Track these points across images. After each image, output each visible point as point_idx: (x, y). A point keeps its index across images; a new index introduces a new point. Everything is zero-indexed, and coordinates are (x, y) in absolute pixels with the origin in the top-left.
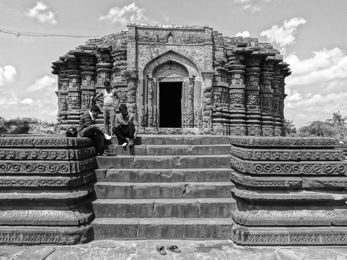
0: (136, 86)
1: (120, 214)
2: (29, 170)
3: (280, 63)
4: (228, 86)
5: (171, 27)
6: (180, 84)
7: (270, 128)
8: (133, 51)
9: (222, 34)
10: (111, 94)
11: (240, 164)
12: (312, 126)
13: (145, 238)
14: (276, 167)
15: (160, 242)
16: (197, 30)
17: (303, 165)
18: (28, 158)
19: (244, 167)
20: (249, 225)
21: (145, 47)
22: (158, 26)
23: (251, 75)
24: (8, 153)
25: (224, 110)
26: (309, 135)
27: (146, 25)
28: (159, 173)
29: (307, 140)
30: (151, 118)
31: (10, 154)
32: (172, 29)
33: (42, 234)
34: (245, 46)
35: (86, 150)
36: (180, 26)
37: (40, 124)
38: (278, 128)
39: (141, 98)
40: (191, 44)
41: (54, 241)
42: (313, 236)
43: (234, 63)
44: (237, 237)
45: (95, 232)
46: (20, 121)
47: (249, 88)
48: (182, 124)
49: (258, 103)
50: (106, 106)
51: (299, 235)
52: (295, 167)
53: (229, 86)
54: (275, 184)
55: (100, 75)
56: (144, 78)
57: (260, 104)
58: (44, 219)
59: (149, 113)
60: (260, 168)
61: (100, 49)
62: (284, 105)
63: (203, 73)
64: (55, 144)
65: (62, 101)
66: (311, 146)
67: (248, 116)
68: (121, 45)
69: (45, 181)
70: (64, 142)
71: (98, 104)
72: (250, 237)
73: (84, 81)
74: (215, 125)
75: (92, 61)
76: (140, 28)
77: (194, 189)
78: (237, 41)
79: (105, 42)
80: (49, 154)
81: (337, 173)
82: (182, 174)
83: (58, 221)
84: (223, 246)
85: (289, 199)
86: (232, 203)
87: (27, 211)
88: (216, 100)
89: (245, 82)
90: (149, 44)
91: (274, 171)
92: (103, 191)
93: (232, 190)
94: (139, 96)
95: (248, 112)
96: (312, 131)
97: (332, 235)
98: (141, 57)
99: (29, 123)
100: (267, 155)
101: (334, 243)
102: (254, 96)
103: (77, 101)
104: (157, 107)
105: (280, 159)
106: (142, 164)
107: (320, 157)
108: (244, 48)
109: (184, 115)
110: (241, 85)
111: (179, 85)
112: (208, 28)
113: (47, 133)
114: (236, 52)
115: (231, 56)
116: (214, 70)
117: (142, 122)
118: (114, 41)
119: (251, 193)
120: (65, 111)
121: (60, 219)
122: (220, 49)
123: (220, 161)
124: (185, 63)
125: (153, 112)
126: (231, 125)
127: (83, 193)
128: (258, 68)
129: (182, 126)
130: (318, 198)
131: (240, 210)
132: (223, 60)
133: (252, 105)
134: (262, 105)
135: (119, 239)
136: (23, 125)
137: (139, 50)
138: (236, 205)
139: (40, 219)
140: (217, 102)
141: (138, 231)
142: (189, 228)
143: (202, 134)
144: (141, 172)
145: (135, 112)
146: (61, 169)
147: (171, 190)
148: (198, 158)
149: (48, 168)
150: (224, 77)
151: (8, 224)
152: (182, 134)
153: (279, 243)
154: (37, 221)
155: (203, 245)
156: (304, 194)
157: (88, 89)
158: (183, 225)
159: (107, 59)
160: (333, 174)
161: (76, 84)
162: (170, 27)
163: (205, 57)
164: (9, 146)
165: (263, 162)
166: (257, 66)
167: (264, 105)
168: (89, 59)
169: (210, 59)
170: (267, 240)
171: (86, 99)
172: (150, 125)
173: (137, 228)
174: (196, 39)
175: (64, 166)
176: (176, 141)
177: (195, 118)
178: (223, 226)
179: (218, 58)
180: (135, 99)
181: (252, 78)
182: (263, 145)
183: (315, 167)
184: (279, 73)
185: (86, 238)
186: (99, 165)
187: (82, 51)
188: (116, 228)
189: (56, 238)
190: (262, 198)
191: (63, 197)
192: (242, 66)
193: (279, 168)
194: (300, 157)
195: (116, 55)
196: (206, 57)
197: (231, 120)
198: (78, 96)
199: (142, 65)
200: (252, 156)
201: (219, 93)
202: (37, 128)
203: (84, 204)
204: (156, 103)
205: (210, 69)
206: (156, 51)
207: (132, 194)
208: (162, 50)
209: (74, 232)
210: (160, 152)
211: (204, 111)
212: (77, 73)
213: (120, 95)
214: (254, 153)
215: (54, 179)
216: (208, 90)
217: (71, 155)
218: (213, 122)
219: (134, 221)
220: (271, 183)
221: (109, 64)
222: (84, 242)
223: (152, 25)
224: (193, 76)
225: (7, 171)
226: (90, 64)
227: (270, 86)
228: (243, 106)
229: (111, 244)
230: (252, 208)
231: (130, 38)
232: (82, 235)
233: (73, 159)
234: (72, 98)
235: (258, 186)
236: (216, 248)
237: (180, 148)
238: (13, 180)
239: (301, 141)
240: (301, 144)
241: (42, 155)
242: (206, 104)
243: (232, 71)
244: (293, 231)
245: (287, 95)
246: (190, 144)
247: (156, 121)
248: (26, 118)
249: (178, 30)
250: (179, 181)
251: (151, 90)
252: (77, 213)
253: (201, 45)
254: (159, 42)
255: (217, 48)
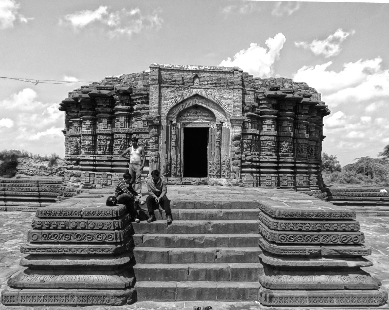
0: (159, 132)
1: (159, 277)
2: (78, 239)
3: (318, 105)
4: (259, 133)
5: (198, 69)
6: (207, 129)
7: (305, 178)
8: (155, 95)
9: (252, 76)
10: (138, 151)
11: (267, 232)
12: (359, 164)
13: (182, 300)
14: (299, 237)
15: (195, 303)
16: (225, 72)
17: (323, 235)
18: (77, 228)
19: (270, 236)
20: (274, 288)
21: (168, 90)
22: (183, 67)
23: (284, 120)
24: (59, 224)
25: (254, 159)
26: (356, 175)
27: (170, 66)
28: (192, 239)
29: (327, 213)
30: (175, 167)
31: (62, 225)
32: (199, 71)
33: (94, 296)
34: (277, 89)
35: (125, 218)
36: (207, 67)
37: (31, 158)
38: (314, 176)
39: (165, 145)
40: (219, 88)
41: (104, 302)
42: (329, 298)
43: (265, 107)
44: (263, 299)
45: (138, 294)
46: (7, 155)
47: (282, 134)
48: (209, 173)
49: (291, 150)
50: (132, 165)
51: (316, 298)
52: (316, 237)
53: (260, 132)
54: (297, 253)
55: (119, 119)
56: (167, 124)
57: (293, 151)
58: (94, 283)
59: (173, 162)
60: (285, 238)
61: (119, 91)
62: (322, 148)
63: (231, 120)
64: (101, 215)
65: (73, 144)
66: (330, 218)
67: (280, 165)
68: (142, 87)
69: (94, 249)
70: (109, 213)
71: (116, 151)
72: (275, 299)
73: (101, 124)
74: (244, 176)
75: (109, 103)
76: (163, 69)
77: (225, 255)
78: (269, 83)
79: (124, 82)
80: (96, 225)
81: (352, 243)
82: (214, 240)
83: (107, 285)
84: (251, 307)
85: (309, 265)
86: (260, 268)
87: (78, 276)
88: (245, 148)
89: (277, 129)
90: (173, 87)
91: (297, 240)
92: (142, 256)
93: (260, 256)
94: (161, 143)
95: (281, 160)
96: (359, 169)
97: (345, 297)
98: (164, 100)
99: (18, 157)
100: (291, 226)
101: (346, 304)
102: (287, 143)
103: (91, 145)
104: (181, 155)
105: (303, 230)
106: (176, 230)
107: (338, 228)
108: (276, 92)
109: (210, 164)
110: (273, 132)
111: (205, 131)
112: (237, 70)
113: (40, 169)
114: (268, 96)
115: (263, 99)
116: (243, 115)
117: (165, 172)
118: (135, 82)
119: (276, 260)
120: (76, 155)
121: (109, 283)
122: (250, 92)
123: (249, 226)
124: (213, 108)
125: (177, 161)
126: (262, 175)
127: (125, 260)
128: (292, 113)
129: (208, 176)
130: (334, 265)
131: (267, 275)
132: (253, 105)
133: (285, 153)
134: (296, 151)
135: (159, 300)
136: (10, 160)
137: (162, 93)
138: (263, 270)
139: (91, 283)
140: (246, 151)
141: (176, 294)
142: (221, 291)
143: (230, 185)
144: (176, 238)
145: (157, 162)
146: (107, 238)
147: (204, 255)
148: (228, 224)
149: (96, 237)
150: (254, 123)
151: (63, 287)
152: (208, 185)
153: (299, 304)
154: (88, 285)
155: (234, 305)
156: (323, 261)
157: (105, 133)
158: (216, 288)
159: (126, 102)
160: (349, 243)
161: (90, 126)
162: (196, 69)
163: (234, 102)
164: (59, 216)
165: (287, 233)
166: (291, 110)
167: (298, 151)
168: (106, 100)
169: (240, 104)
170: (289, 301)
171: (102, 145)
172: (173, 175)
173: (175, 291)
174: (224, 82)
175: (110, 235)
176: (206, 205)
177: (222, 168)
178: (251, 289)
179: (248, 103)
180: (158, 147)
181: (285, 124)
182: (288, 217)
183: (333, 238)
184: (315, 115)
185: (131, 300)
186: (135, 231)
187: (99, 92)
188: (157, 290)
189: (105, 300)
190: (285, 265)
191: (111, 263)
192: (275, 111)
193: (301, 238)
194: (320, 228)
195: (137, 98)
196: (235, 103)
197: (262, 170)
198: (92, 140)
199: (166, 109)
200: (277, 227)
201: (249, 141)
202: (27, 163)
203: (126, 270)
204: (180, 150)
205: (239, 115)
206: (181, 95)
207: (168, 259)
208: (187, 93)
209: (122, 295)
210: (192, 217)
211: (232, 160)
212: (91, 114)
213: (141, 143)
214: (279, 224)
215: (102, 248)
216: (237, 138)
217: (115, 225)
218: (242, 172)
219: (172, 284)
220: (294, 251)
221: (128, 107)
222: (130, 303)
223: (177, 66)
224: (221, 122)
225: (60, 240)
226: (107, 106)
227: (305, 131)
228: (274, 155)
229: (153, 305)
230: (277, 273)
231: (153, 80)
232: (129, 297)
233: (117, 229)
234: (85, 142)
235: (282, 254)
236: (245, 308)
237: (211, 214)
238: (65, 248)
239: (322, 214)
240: (321, 217)
241: (90, 225)
242: (234, 153)
243: (263, 116)
244: (312, 294)
245: (325, 137)
246: (220, 209)
247: (180, 170)
248: (14, 151)
249: (205, 72)
250: (211, 246)
251: (175, 137)
252: (122, 277)
253: (230, 89)
254: (184, 85)
255: (247, 92)
